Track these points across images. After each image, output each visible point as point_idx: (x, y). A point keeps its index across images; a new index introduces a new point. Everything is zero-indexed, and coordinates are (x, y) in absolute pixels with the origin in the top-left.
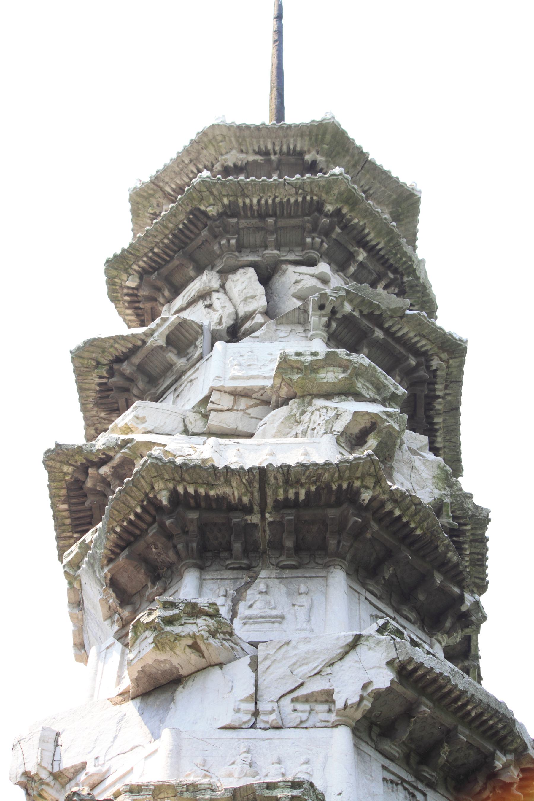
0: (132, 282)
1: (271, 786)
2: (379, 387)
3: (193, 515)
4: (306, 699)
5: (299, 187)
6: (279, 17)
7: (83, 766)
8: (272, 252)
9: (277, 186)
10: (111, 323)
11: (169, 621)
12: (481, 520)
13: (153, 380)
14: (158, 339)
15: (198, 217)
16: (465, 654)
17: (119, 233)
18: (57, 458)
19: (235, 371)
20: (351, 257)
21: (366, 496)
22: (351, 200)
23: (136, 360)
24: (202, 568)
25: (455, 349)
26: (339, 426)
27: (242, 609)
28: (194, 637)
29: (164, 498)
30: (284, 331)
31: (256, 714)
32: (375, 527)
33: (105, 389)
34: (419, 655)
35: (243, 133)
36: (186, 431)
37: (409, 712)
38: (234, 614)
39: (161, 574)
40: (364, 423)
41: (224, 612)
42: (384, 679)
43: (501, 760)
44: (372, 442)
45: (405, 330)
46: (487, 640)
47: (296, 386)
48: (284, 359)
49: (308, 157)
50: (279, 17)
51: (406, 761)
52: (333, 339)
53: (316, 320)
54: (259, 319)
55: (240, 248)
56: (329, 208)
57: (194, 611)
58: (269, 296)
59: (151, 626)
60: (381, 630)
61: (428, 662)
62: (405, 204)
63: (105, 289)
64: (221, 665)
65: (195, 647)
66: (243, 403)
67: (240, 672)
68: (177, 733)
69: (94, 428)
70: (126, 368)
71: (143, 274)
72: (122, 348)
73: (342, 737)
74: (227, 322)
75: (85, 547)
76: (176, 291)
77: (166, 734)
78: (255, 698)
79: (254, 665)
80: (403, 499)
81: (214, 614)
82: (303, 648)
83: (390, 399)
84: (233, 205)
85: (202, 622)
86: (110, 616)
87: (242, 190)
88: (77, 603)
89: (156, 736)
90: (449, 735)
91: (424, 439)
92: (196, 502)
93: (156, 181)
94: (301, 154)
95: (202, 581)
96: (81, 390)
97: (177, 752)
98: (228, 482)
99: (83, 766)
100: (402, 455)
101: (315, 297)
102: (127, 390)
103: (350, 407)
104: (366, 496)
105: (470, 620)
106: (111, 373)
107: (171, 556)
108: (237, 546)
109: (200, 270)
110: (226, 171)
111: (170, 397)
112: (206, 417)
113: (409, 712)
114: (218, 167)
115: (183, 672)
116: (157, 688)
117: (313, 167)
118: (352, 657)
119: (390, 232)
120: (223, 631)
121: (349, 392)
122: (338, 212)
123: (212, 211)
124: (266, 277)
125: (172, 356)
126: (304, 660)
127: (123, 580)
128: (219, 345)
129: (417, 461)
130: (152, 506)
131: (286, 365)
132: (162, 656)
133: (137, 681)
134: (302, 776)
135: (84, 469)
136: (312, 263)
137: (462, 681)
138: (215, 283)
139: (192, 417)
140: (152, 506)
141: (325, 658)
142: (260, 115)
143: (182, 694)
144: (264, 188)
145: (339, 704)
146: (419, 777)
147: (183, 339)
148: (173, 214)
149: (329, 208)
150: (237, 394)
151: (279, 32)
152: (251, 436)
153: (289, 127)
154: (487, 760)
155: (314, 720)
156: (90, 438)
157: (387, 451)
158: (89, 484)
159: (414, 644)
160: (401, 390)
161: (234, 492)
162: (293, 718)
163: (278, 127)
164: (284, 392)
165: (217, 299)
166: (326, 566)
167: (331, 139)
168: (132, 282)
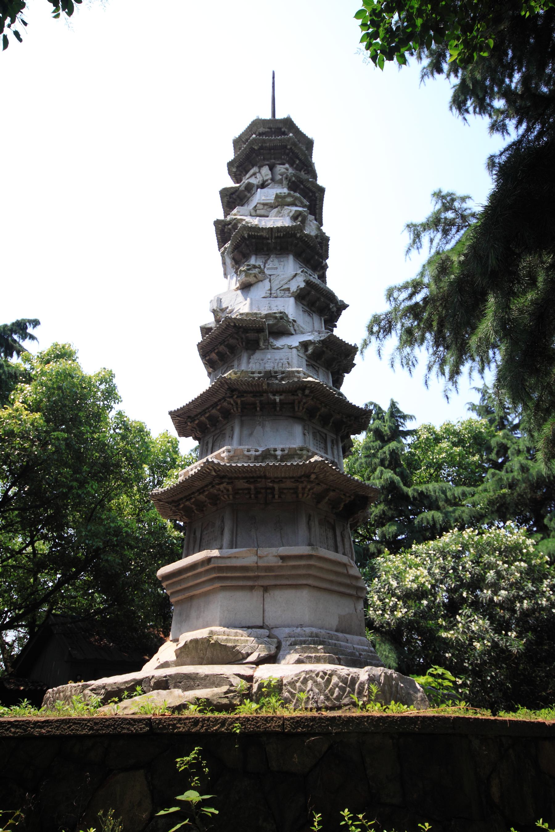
0: (234, 170)
1: (275, 313)
2: (302, 203)
3: (254, 240)
4: (283, 290)
5: (280, 140)
6: (274, 78)
7: (228, 307)
9: (274, 140)
10: (230, 183)
11: (248, 270)
12: (327, 239)
13: (241, 200)
14: (242, 188)
15: (252, 150)
16: (323, 277)
17: (230, 155)
18: (217, 223)
19: (263, 198)
20: (294, 162)
21: (298, 235)
22: (294, 144)
23: (237, 194)
24: (256, 255)
25: (322, 190)
26: (291, 214)
27: (267, 266)
29: (246, 236)
30: (276, 186)
31: (271, 294)
32: (300, 243)
33: (228, 202)
34: (311, 278)
35: (263, 122)
36: (251, 215)
37: (309, 293)
38: (265, 267)
39: (246, 257)
40: (298, 213)
41: (262, 267)
42: (303, 285)
43: (331, 306)
44: (300, 219)
45: (309, 185)
46: (328, 273)
47: (280, 202)
48: (277, 194)
49: (283, 130)
50: (274, 78)
51: (308, 306)
52: (290, 188)
53: (285, 182)
54: (269, 181)
55: (264, 159)
56: (289, 147)
57: (255, 267)
58: (272, 174)
59: (244, 271)
60: (302, 272)
61: (314, 280)
62: (309, 144)
63: (227, 171)
65: (255, 276)
66: (266, 207)
67: (267, 282)
68: (251, 299)
69: (226, 214)
70: (234, 196)
71: (237, 167)
72: (233, 190)
73: (292, 300)
74: (261, 182)
75: (226, 248)
76: (247, 172)
77: (248, 299)
78: (270, 290)
79: (270, 281)
80: (307, 236)
81: (260, 268)
82: (282, 277)
83: (304, 207)
84: (262, 146)
85: (257, 270)
86: (233, 267)
87: (264, 141)
88: (224, 263)
89: (246, 300)
90: (319, 299)
91: (313, 217)
92: (254, 237)
93: (240, 137)
94: (281, 129)
95: (256, 258)
97: (251, 304)
99: (228, 307)
100: (308, 222)
101: (285, 176)
102: (234, 203)
103: (294, 209)
104: (298, 235)
105: (325, 267)
106: (230, 198)
107: (248, 251)
108: (265, 249)
109: (253, 167)
110: (260, 134)
111: (246, 205)
112: (256, 211)
113: (309, 293)
114: (257, 133)
116: (245, 287)
117: (284, 133)
118: (295, 279)
119: (305, 154)
120: (262, 272)
121: (293, 204)
122: (291, 148)
123: (256, 148)
124: (271, 168)
125: (246, 193)
126: (283, 280)
127: (236, 257)
128: (259, 190)
129: (311, 224)
130: (243, 238)
131: (277, 197)
132: (247, 279)
133: (240, 285)
134: (282, 310)
136: (284, 164)
137: (322, 286)
138: (257, 171)
139: (252, 211)
140: (243, 238)
141: (288, 279)
142: (268, 116)
143: (252, 289)
144: (271, 141)
145: (291, 291)
146: (311, 310)
147: (249, 188)
148: (245, 149)
149: (289, 147)
150: (264, 204)
151: (273, 83)
152: (268, 217)
153: (278, 120)
154: (328, 305)
155: (285, 295)
156: (225, 216)
157: (303, 221)
158: (226, 230)
159: (310, 275)
160: (308, 203)
161: (264, 234)
162: (280, 295)
163: (273, 120)
164: (277, 204)
165: (258, 175)
166: (288, 254)
167: (288, 123)
168: (234, 170)
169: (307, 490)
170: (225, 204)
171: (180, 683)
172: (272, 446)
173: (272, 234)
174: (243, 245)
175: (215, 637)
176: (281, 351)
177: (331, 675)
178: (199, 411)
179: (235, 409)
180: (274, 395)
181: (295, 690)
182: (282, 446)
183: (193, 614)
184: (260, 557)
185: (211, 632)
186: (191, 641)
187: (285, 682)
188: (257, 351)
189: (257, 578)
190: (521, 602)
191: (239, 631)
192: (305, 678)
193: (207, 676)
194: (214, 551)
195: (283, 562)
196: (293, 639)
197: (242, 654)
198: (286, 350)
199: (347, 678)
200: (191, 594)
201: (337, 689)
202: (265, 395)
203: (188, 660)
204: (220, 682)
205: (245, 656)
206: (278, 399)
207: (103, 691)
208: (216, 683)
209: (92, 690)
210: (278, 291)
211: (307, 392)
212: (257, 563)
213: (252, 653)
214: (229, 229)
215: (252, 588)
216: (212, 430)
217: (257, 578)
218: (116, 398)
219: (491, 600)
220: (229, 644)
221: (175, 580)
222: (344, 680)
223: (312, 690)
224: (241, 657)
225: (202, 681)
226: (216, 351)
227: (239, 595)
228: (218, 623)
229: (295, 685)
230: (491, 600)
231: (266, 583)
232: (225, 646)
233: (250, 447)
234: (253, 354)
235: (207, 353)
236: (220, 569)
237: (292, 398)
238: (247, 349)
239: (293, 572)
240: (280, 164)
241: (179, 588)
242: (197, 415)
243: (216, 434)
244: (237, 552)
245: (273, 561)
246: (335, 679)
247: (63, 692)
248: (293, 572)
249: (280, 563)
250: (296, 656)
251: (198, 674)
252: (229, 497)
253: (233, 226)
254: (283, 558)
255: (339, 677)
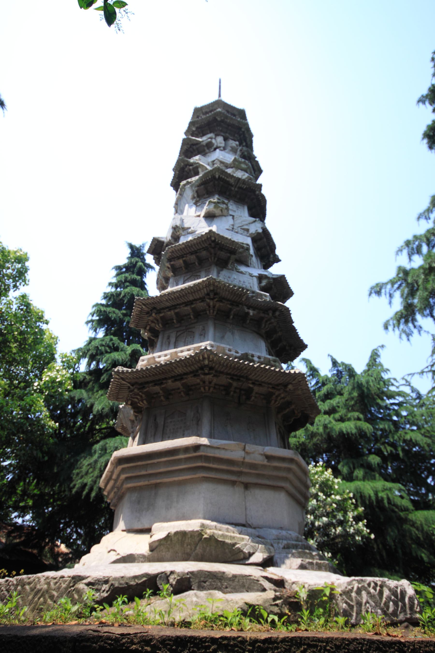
0: (194, 129)
3: (222, 183)
4: (243, 229)
6: (220, 83)
8: (227, 135)
11: (218, 203)
19: (221, 157)
23: (197, 146)
28: (222, 208)
29: (217, 176)
31: (233, 228)
50: (220, 83)
58: (225, 144)
59: (214, 203)
64: (225, 216)
65: (221, 210)
70: (195, 147)
71: (197, 128)
87: (227, 117)
93: (202, 108)
96: (181, 148)
98: (231, 178)
99: (190, 228)
106: (190, 147)
109: (211, 132)
113: (261, 239)
115: (216, 215)
123: (219, 119)
125: (206, 148)
126: (244, 221)
132: (214, 210)
135: (186, 165)
143: (216, 220)
158: (186, 169)
161: (232, 181)
164: (232, 165)
168: (194, 129)
169: (279, 398)
170: (183, 151)
171: (205, 582)
172: (250, 352)
173: (237, 183)
174: (211, 183)
175: (208, 531)
176: (244, 275)
177: (381, 586)
178: (168, 304)
179: (211, 311)
180: (248, 309)
181: (352, 600)
182: (258, 354)
183: (160, 502)
184: (247, 453)
185: (203, 525)
186: (176, 533)
187: (110, 579)
188: (225, 270)
189: (240, 473)
190: (335, 528)
191: (230, 527)
192: (358, 588)
193: (235, 576)
194: (203, 439)
195: (268, 462)
196: (285, 542)
197: (244, 553)
198: (247, 276)
199: (396, 591)
200: (158, 481)
201: (391, 603)
202: (240, 306)
203: (169, 555)
204: (250, 584)
205: (247, 555)
206: (251, 312)
207: (105, 587)
208: (247, 585)
209: (88, 584)
210: (239, 228)
211: (277, 313)
212: (244, 458)
213: (253, 553)
214: (190, 170)
215: (233, 483)
216: (176, 326)
217: (240, 473)
218: (24, 281)
219: (313, 523)
220: (228, 541)
221: (139, 463)
222: (393, 592)
223: (368, 603)
224: (242, 556)
225: (231, 583)
226: (184, 259)
227: (222, 489)
228: (201, 515)
229: (350, 596)
230: (313, 523)
231: (244, 479)
232: (224, 542)
233: (231, 347)
234: (222, 270)
235: (173, 258)
236: (207, 459)
237: (262, 315)
238: (217, 265)
239: (275, 473)
240: (232, 140)
241: (143, 473)
242: (163, 309)
243: (180, 331)
244: (225, 444)
245: (260, 460)
246: (386, 593)
247: (29, 583)
248: (275, 473)
249: (265, 462)
250: (299, 561)
251: (224, 573)
252: (209, 389)
253: (193, 168)
254: (269, 458)
255: (390, 590)
